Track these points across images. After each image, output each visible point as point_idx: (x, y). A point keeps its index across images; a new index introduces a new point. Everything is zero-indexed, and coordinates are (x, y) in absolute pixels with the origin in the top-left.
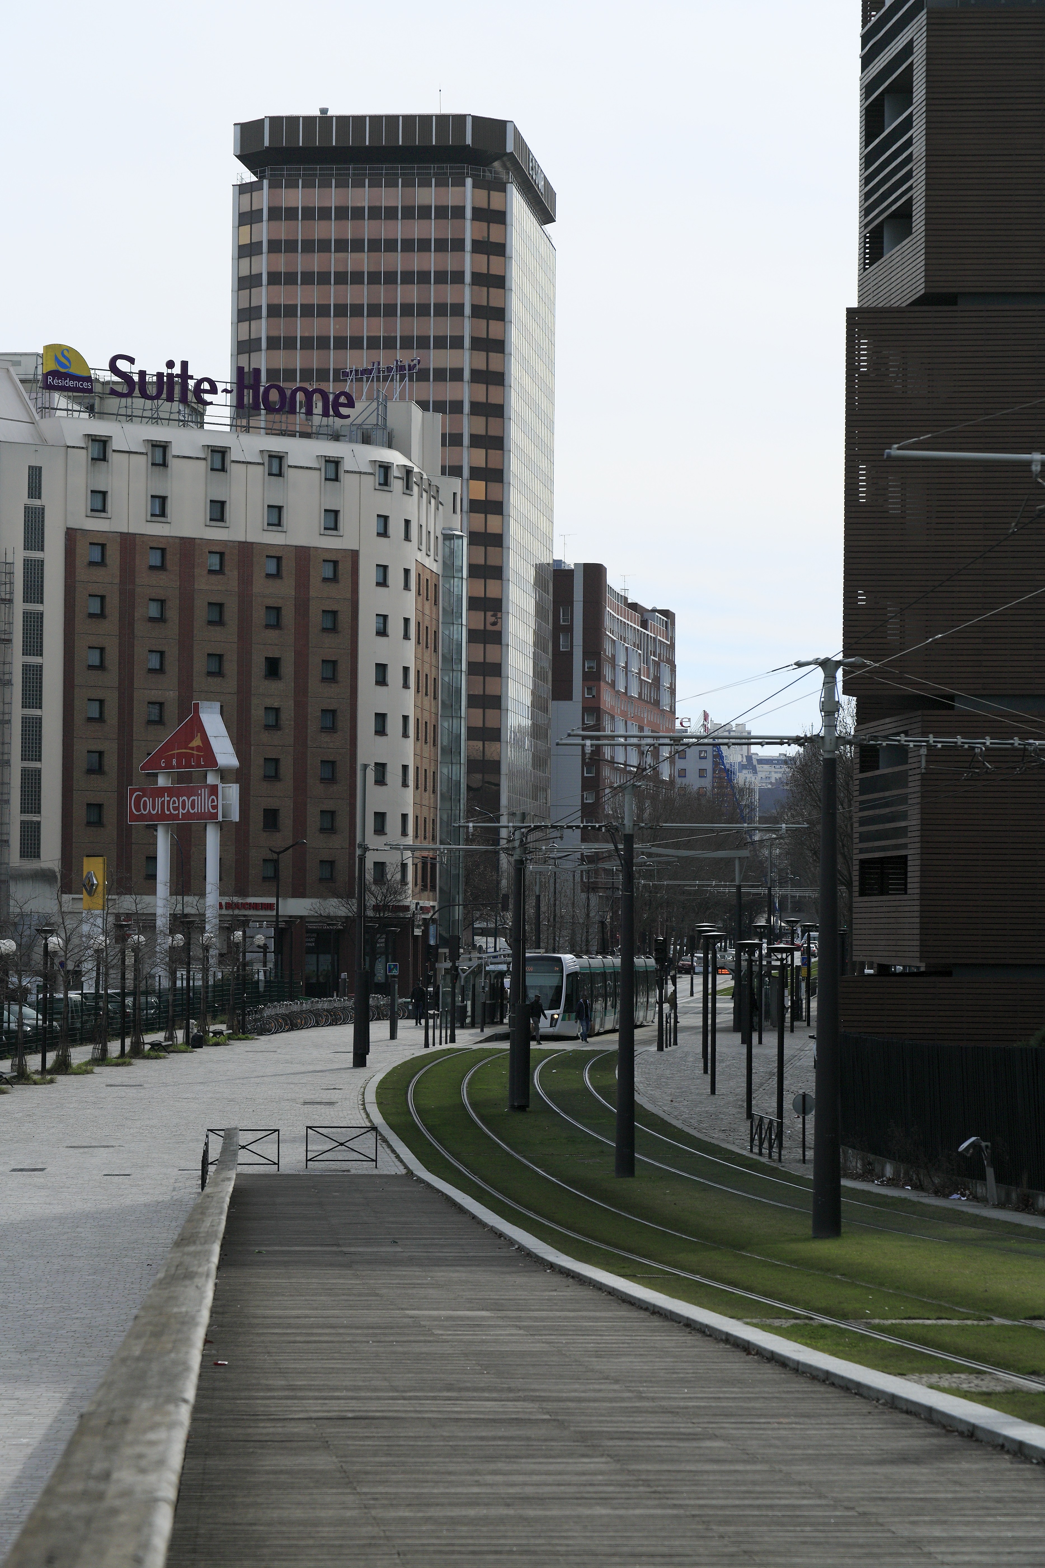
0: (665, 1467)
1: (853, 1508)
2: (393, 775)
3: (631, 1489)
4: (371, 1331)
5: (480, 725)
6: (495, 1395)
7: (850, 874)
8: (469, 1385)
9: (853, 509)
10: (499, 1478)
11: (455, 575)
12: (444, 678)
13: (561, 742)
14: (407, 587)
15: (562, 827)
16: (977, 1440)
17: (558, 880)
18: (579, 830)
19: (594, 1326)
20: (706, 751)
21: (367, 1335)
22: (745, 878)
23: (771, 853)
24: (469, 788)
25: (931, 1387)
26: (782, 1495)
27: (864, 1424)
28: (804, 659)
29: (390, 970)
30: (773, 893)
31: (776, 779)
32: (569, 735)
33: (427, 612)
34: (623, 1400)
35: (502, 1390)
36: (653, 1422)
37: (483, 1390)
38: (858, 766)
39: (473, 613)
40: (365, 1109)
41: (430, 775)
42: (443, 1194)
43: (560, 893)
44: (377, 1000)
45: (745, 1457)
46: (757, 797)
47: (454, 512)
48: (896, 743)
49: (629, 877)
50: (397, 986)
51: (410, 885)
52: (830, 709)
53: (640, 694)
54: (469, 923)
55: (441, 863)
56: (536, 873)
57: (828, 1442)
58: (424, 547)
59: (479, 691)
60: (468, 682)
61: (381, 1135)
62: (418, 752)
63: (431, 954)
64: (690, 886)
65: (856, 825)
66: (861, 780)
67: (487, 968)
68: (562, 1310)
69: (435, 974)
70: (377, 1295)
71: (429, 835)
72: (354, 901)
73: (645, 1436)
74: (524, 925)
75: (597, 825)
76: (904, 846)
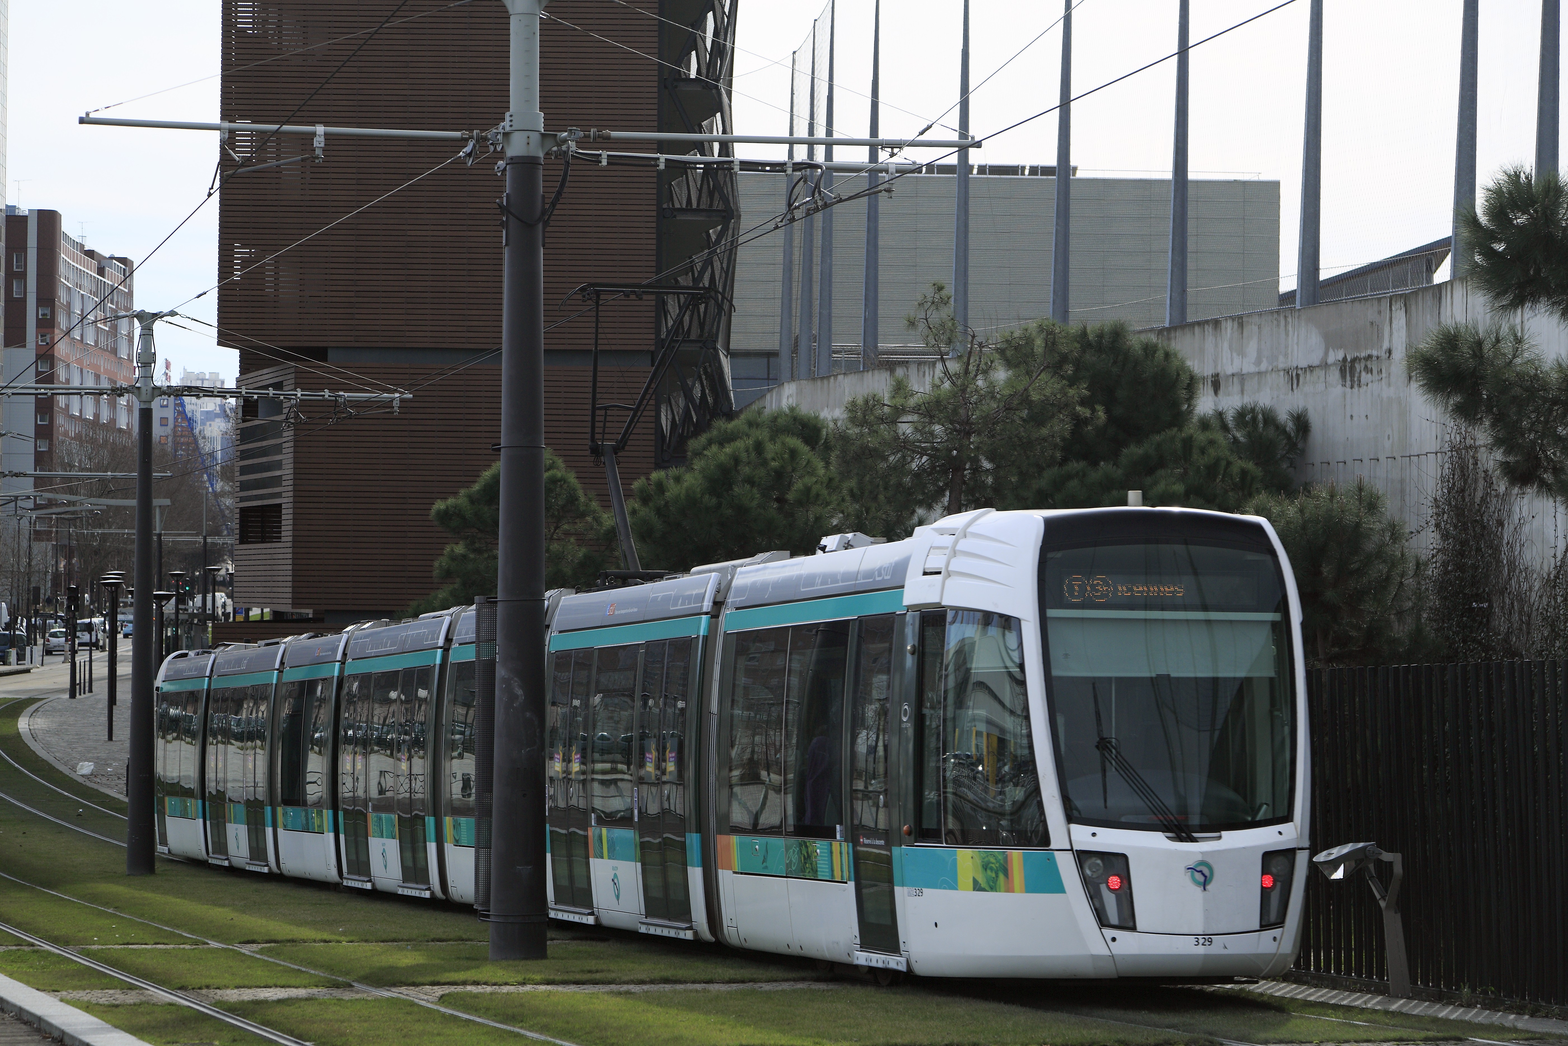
53: (96, 342)
76: (279, 495)
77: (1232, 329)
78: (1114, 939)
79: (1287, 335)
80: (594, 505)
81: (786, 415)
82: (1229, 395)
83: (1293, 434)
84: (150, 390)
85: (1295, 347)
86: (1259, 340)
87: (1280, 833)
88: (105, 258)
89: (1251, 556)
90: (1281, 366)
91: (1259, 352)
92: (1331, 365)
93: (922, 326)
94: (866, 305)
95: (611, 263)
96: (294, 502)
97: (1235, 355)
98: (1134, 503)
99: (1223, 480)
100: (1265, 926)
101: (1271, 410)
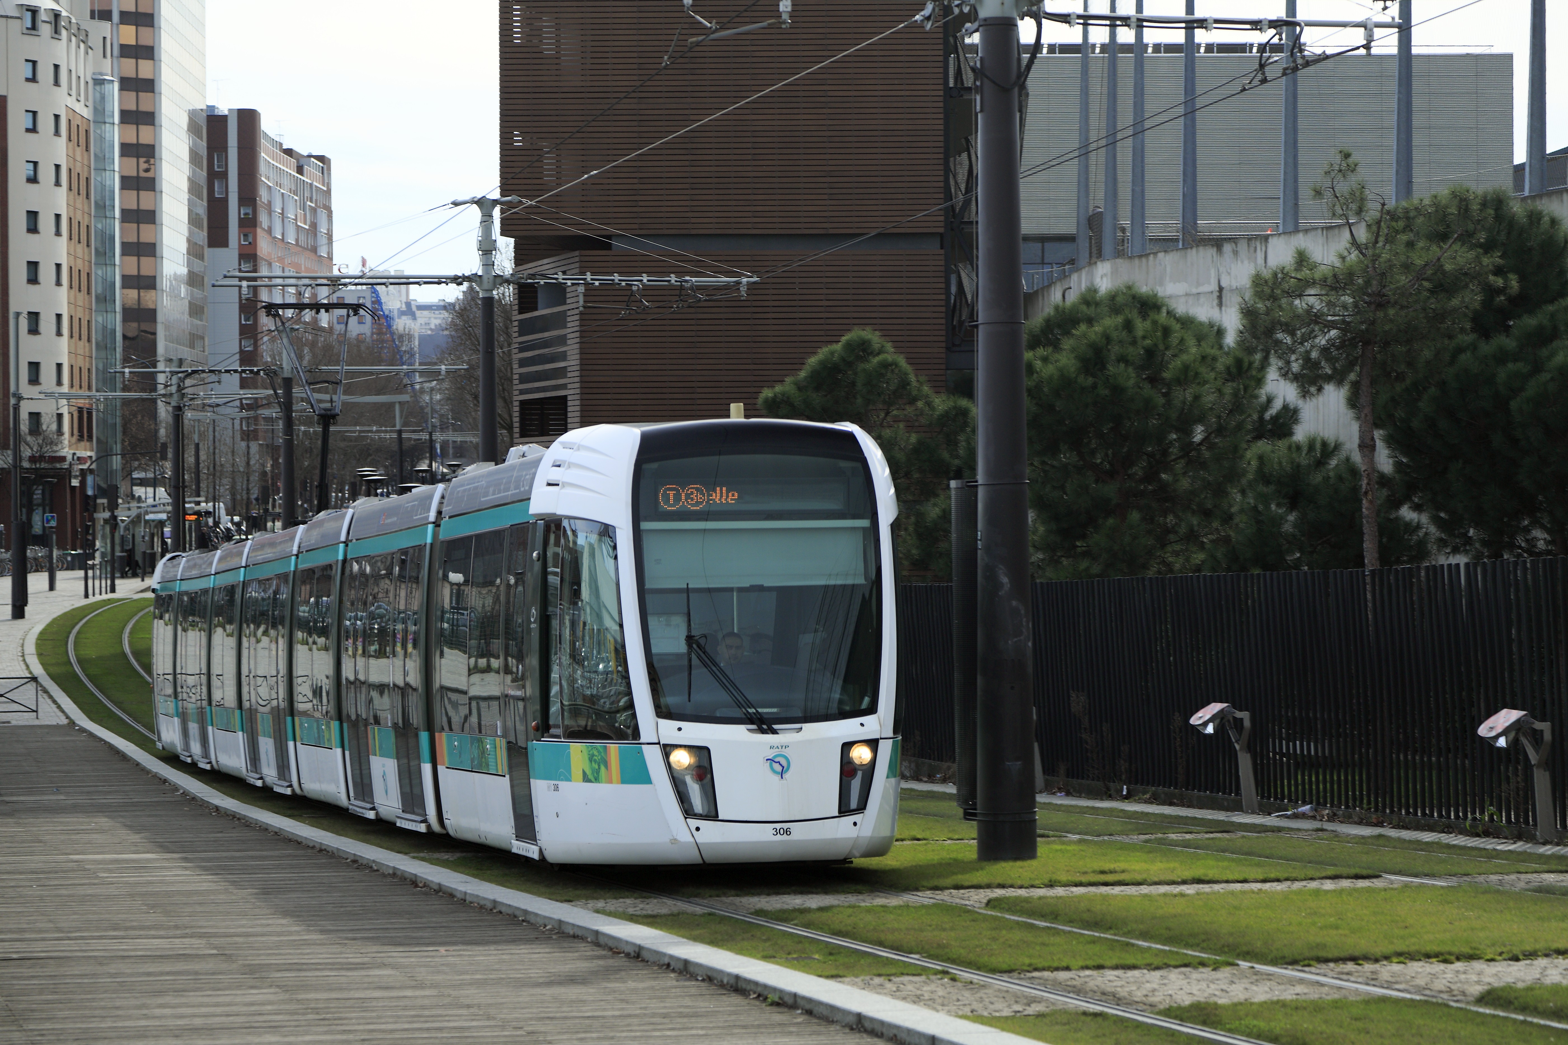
0: (334, 995)
1: (521, 1028)
2: (47, 324)
3: (300, 1017)
4: (34, 876)
5: (135, 273)
6: (162, 933)
7: (511, 416)
8: (135, 924)
9: (508, 50)
10: (168, 1011)
11: (107, 120)
12: (97, 225)
14: (57, 133)
15: (220, 371)
16: (643, 961)
17: (217, 428)
21: (31, 880)
22: (405, 424)
23: (431, 399)
24: (125, 337)
25: (597, 911)
28: (460, 199)
29: (48, 521)
32: (225, 277)
33: (79, 158)
34: (290, 933)
35: (169, 928)
37: (149, 928)
38: (516, 307)
39: (125, 159)
40: (24, 660)
41: (84, 324)
42: (106, 742)
43: (220, 441)
44: (34, 552)
45: (414, 983)
47: (105, 56)
50: (54, 537)
51: (67, 435)
52: (487, 249)
53: (297, 240)
54: (127, 473)
55: (98, 411)
57: (497, 967)
58: (74, 93)
59: (133, 239)
60: (122, 230)
61: (41, 686)
62: (72, 301)
63: (88, 505)
65: (515, 366)
66: (520, 321)
67: (147, 517)
68: (228, 851)
69: (94, 525)
70: (40, 841)
71: (85, 384)
72: (9, 452)
74: (183, 475)
75: (255, 369)
76: (564, 387)
80: (926, 389)
81: (1123, 294)
84: (492, 278)
87: (862, 725)
88: (303, 156)
89: (843, 464)
93: (1328, 194)
96: (582, 394)
98: (736, 415)
100: (844, 810)
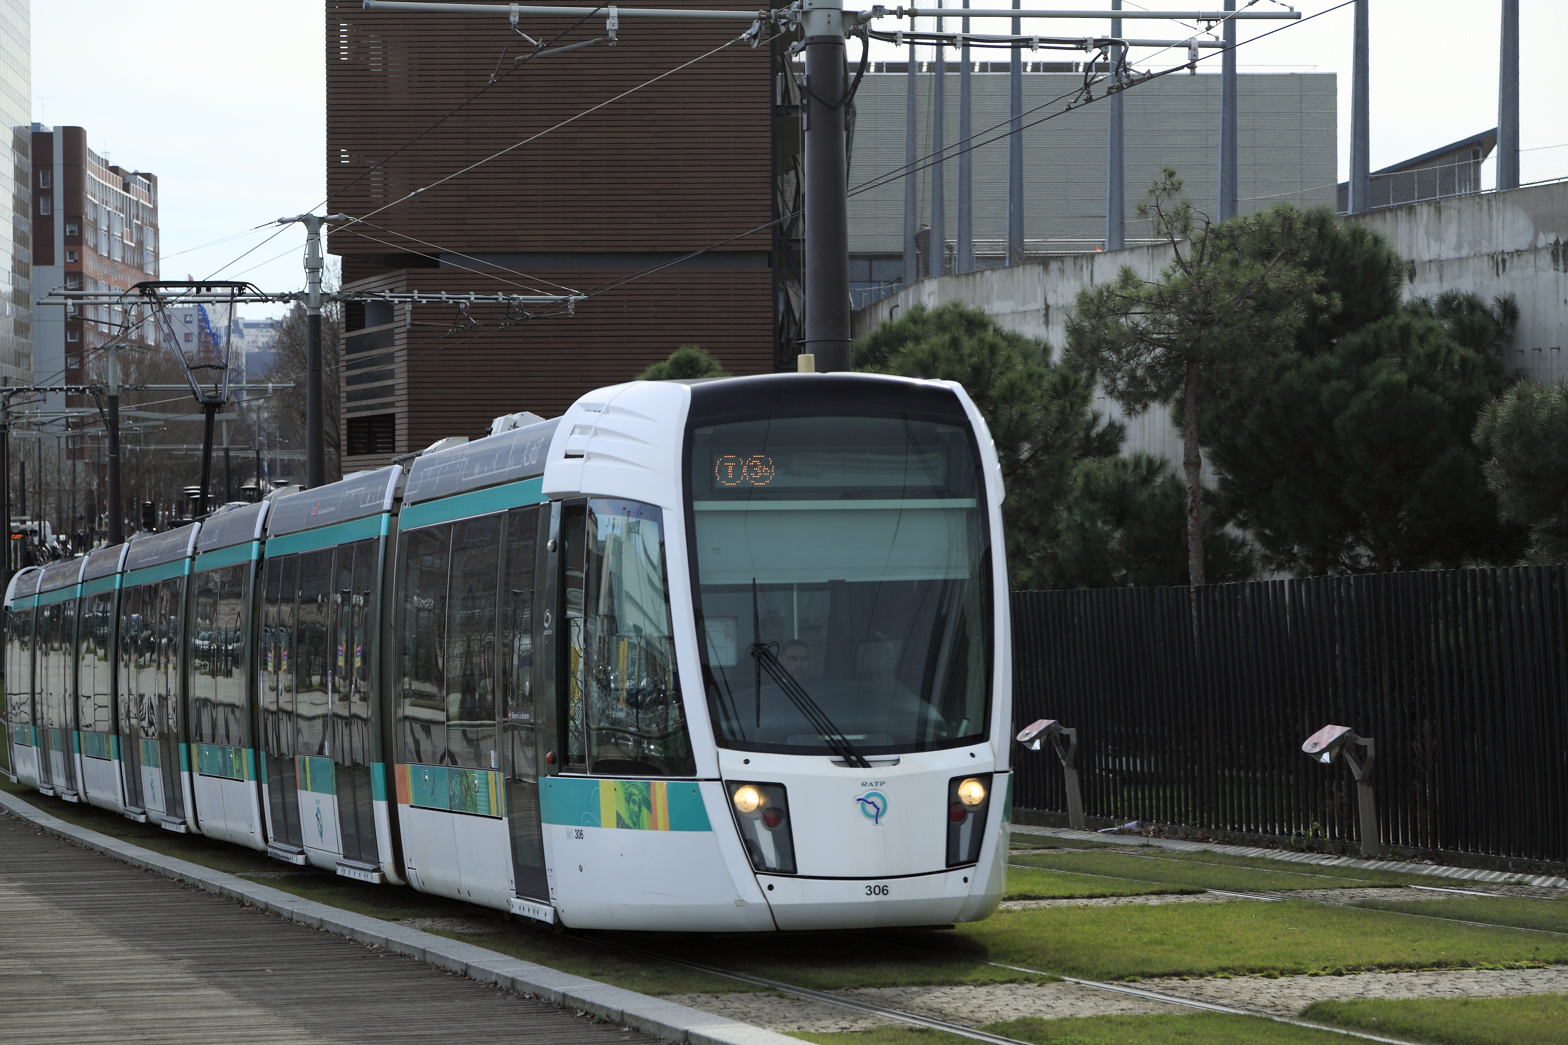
7: (339, 435)
9: (334, 67)
13: (42, 301)
15: (45, 390)
17: (43, 447)
18: (63, 393)
19: (85, 885)
20: (191, 316)
22: (233, 442)
23: (258, 417)
25: (424, 930)
26: (277, 1038)
27: (359, 968)
28: (287, 216)
30: (261, 456)
31: (263, 343)
34: (116, 954)
36: (147, 974)
38: (344, 325)
43: (45, 459)
46: (244, 361)
48: (381, 299)
49: (115, 442)
52: (314, 267)
53: (123, 258)
56: (20, 439)
64: (178, 450)
65: (343, 384)
66: (347, 339)
68: (53, 871)
73: (139, 987)
74: (9, 493)
75: (81, 388)
76: (392, 405)
77: (1429, 214)
78: (771, 887)
79: (1491, 219)
82: (1426, 282)
83: (1501, 321)
85: (1501, 231)
86: (1460, 224)
87: (972, 755)
90: (1485, 251)
91: (1459, 236)
92: (1542, 249)
94: (1011, 199)
95: (726, 163)
96: (409, 412)
97: (1432, 241)
99: (1443, 369)
100: (953, 863)
101: (1474, 296)
